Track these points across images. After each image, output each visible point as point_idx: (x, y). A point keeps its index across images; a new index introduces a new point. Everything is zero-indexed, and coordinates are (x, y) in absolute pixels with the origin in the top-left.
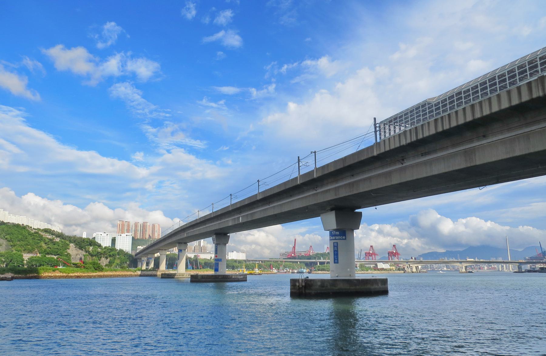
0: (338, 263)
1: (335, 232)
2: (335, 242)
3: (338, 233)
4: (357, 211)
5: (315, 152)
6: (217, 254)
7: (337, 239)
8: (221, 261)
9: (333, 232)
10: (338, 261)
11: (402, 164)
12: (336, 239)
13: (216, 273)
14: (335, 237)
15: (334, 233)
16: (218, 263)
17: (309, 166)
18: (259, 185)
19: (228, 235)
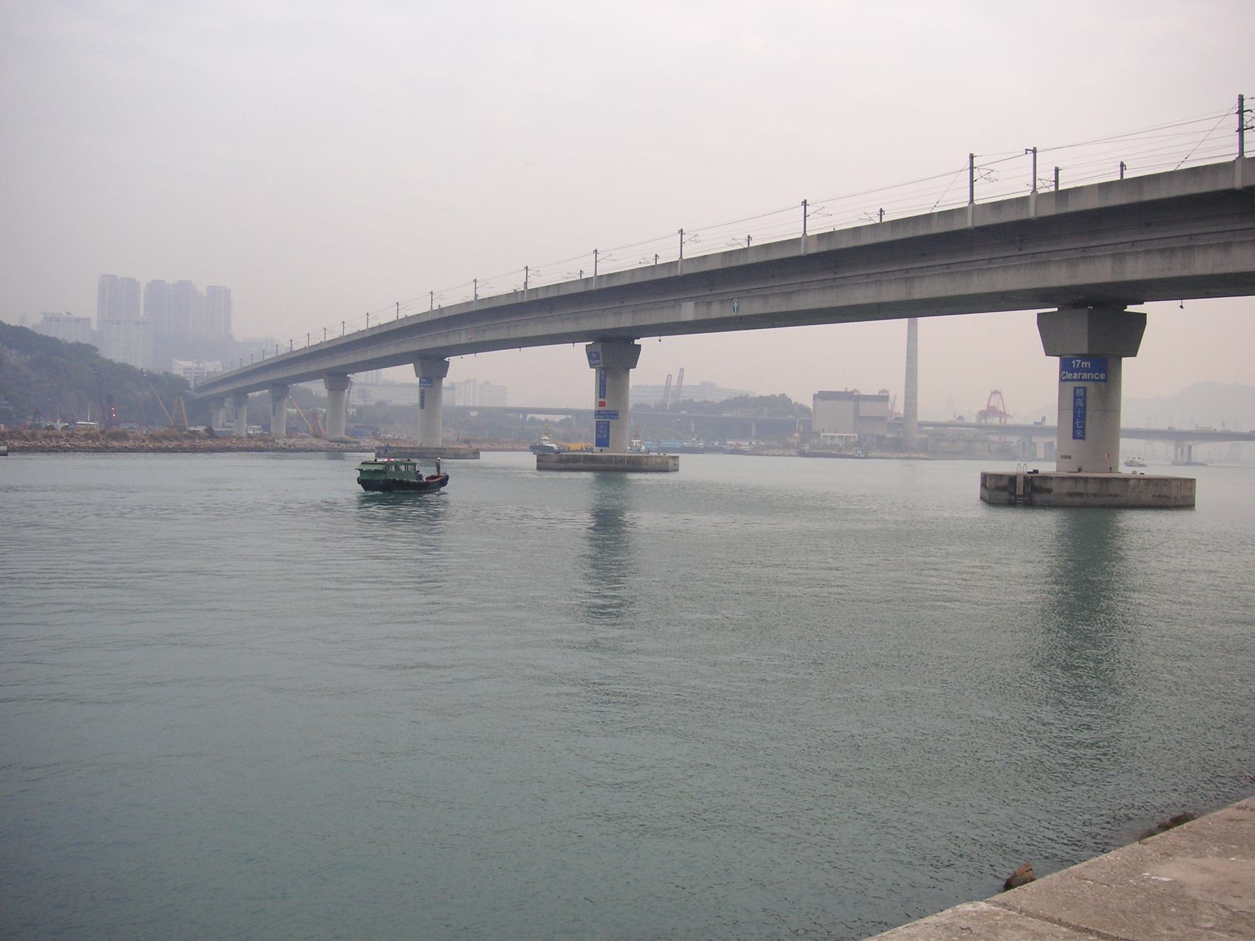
0: (1083, 438)
1: (1079, 361)
2: (1079, 388)
3: (1087, 364)
4: (1131, 308)
5: (1034, 151)
6: (604, 398)
7: (1085, 380)
8: (617, 418)
9: (1074, 362)
10: (1084, 434)
11: (836, 274)
12: (1081, 380)
13: (601, 450)
14: (1080, 374)
15: (1076, 363)
16: (609, 422)
17: (700, 241)
18: (681, 241)
19: (447, 359)
